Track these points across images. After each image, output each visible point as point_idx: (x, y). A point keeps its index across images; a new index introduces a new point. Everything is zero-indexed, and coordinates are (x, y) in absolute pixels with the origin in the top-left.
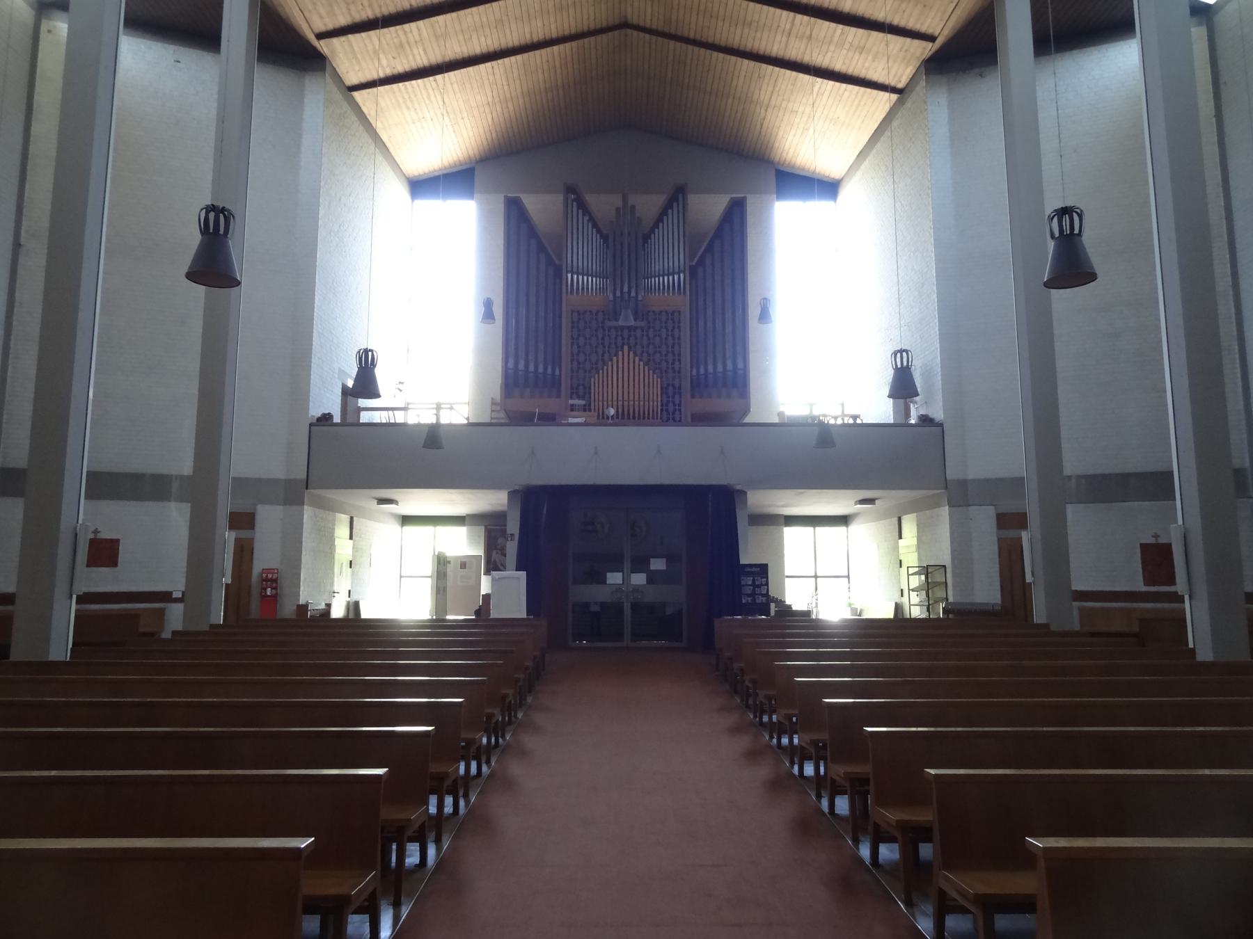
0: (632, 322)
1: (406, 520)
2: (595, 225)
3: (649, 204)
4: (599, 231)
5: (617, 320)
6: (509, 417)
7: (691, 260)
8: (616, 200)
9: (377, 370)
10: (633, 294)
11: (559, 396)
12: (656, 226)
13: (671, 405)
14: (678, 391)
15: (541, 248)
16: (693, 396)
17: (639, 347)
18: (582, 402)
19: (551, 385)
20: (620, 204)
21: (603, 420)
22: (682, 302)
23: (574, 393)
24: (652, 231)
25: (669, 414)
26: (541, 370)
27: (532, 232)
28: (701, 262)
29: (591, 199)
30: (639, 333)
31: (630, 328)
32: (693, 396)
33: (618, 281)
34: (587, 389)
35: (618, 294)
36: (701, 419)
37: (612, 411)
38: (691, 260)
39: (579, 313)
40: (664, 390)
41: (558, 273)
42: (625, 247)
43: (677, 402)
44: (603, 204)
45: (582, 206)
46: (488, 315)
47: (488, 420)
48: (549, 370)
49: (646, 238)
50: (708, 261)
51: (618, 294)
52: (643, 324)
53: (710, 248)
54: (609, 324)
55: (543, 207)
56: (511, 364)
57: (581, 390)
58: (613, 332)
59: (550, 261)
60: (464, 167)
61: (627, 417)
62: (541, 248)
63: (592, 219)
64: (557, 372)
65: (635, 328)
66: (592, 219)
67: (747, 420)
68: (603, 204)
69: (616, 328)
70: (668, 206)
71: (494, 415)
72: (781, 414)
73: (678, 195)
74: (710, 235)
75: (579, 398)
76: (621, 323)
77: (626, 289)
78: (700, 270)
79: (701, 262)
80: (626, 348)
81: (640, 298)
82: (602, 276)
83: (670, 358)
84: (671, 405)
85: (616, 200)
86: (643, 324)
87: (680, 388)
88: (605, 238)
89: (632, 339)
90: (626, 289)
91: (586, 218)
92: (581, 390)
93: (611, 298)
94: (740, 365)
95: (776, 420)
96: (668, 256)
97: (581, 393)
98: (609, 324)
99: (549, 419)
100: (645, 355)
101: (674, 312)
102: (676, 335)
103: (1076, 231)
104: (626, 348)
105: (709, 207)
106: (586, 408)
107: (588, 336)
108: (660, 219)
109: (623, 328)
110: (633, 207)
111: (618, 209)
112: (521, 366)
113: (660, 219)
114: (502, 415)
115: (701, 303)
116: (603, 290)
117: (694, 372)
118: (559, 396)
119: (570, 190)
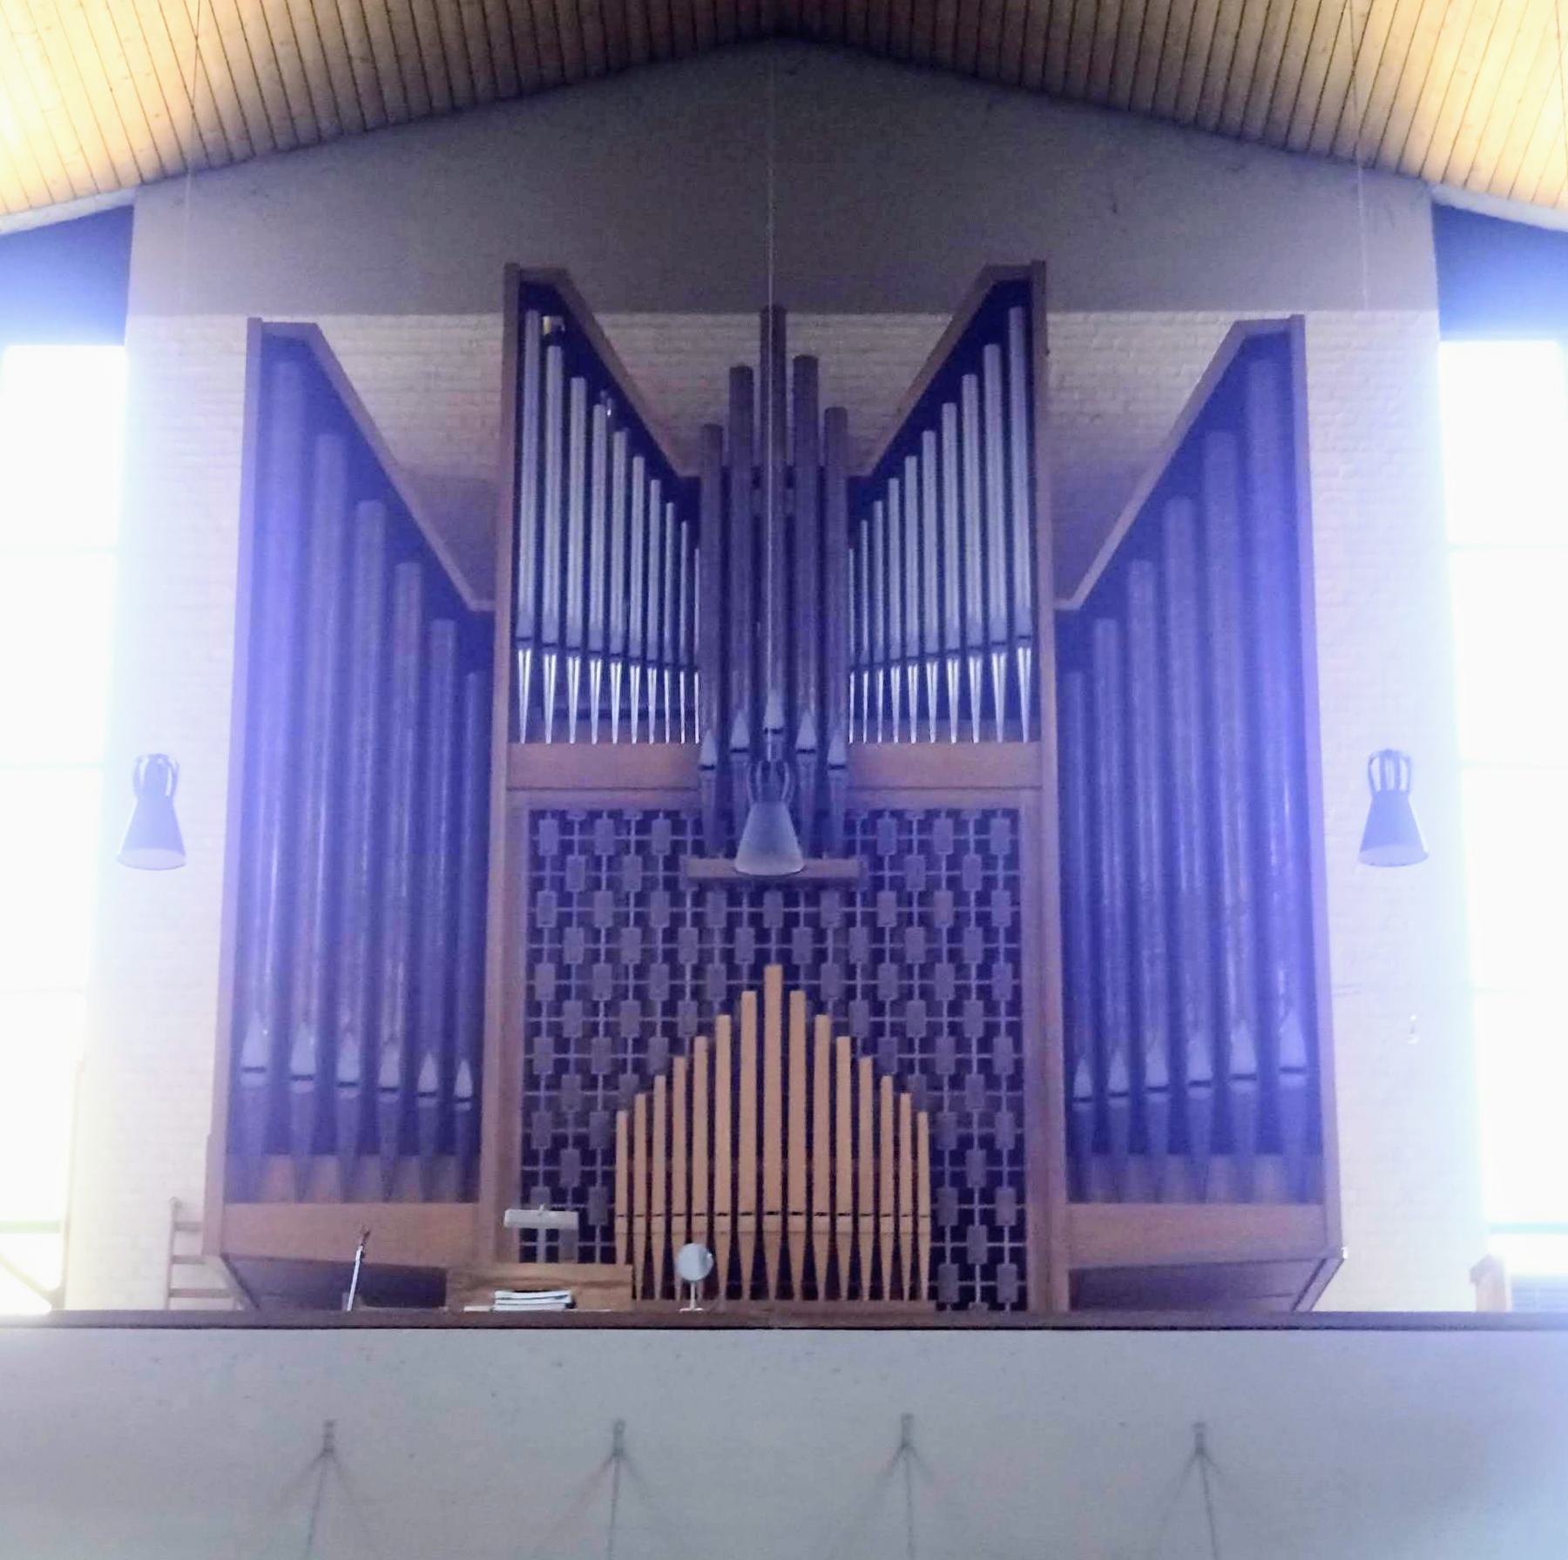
0: (794, 861)
1: (1371, 761)
2: (642, 443)
3: (874, 356)
4: (657, 466)
5: (731, 853)
6: (244, 1287)
7: (1064, 587)
8: (735, 338)
9: (1412, 799)
10: (807, 737)
11: (468, 1191)
12: (907, 442)
13: (978, 1230)
14: (1010, 1167)
15: (405, 541)
16: (1078, 1193)
17: (831, 969)
18: (567, 1220)
19: (440, 1143)
20: (750, 353)
21: (658, 1302)
22: (1014, 770)
23: (537, 1176)
24: (891, 467)
25: (972, 1273)
26: (390, 1072)
27: (367, 472)
28: (1111, 597)
29: (632, 339)
30: (831, 909)
31: (789, 888)
32: (1078, 1193)
33: (740, 678)
34: (598, 1158)
35: (740, 736)
36: (1113, 1298)
37: (691, 1263)
38: (1064, 587)
39: (566, 826)
40: (947, 1163)
41: (477, 648)
42: (768, 525)
43: (1006, 1215)
44: (678, 357)
45: (586, 360)
46: (158, 830)
47: (150, 1299)
48: (429, 1078)
49: (866, 494)
50: (1141, 592)
51: (740, 736)
52: (850, 867)
53: (1145, 540)
54: (697, 867)
55: (421, 369)
56: (257, 1050)
57: (569, 1166)
58: (716, 909)
59: (440, 598)
60: (87, 207)
61: (771, 1284)
62: (405, 541)
63: (627, 417)
64: (464, 1086)
65: (817, 888)
66: (627, 417)
67: (1333, 1299)
68: (678, 357)
69: (733, 889)
70: (960, 359)
71: (183, 1277)
72: (1483, 1273)
73: (1001, 316)
74: (1145, 489)
75: (558, 1199)
76: (745, 864)
77: (773, 717)
78: (1104, 631)
79: (1111, 597)
80: (773, 975)
81: (836, 754)
82: (679, 662)
83: (974, 1017)
84: (978, 1230)
85: (735, 338)
86: (850, 867)
87: (1017, 1155)
88: (682, 497)
89: (802, 933)
90: (773, 717)
91: (603, 413)
92: (569, 1166)
93: (709, 755)
94: (1292, 1050)
95: (1462, 1299)
96: (962, 566)
97: (570, 1178)
98: (697, 867)
99: (413, 1295)
100: (860, 1006)
101: (931, 815)
102: (1001, 915)
103: (1403, 786)
104: (773, 975)
105: (1133, 363)
106: (594, 1243)
107: (603, 920)
108: (924, 417)
109: (760, 887)
110: (807, 364)
111: (741, 376)
112: (304, 1058)
113: (924, 417)
114: (214, 1276)
115: (1110, 776)
116: (679, 719)
117: (1084, 1083)
118: (468, 1191)
119: (534, 294)
